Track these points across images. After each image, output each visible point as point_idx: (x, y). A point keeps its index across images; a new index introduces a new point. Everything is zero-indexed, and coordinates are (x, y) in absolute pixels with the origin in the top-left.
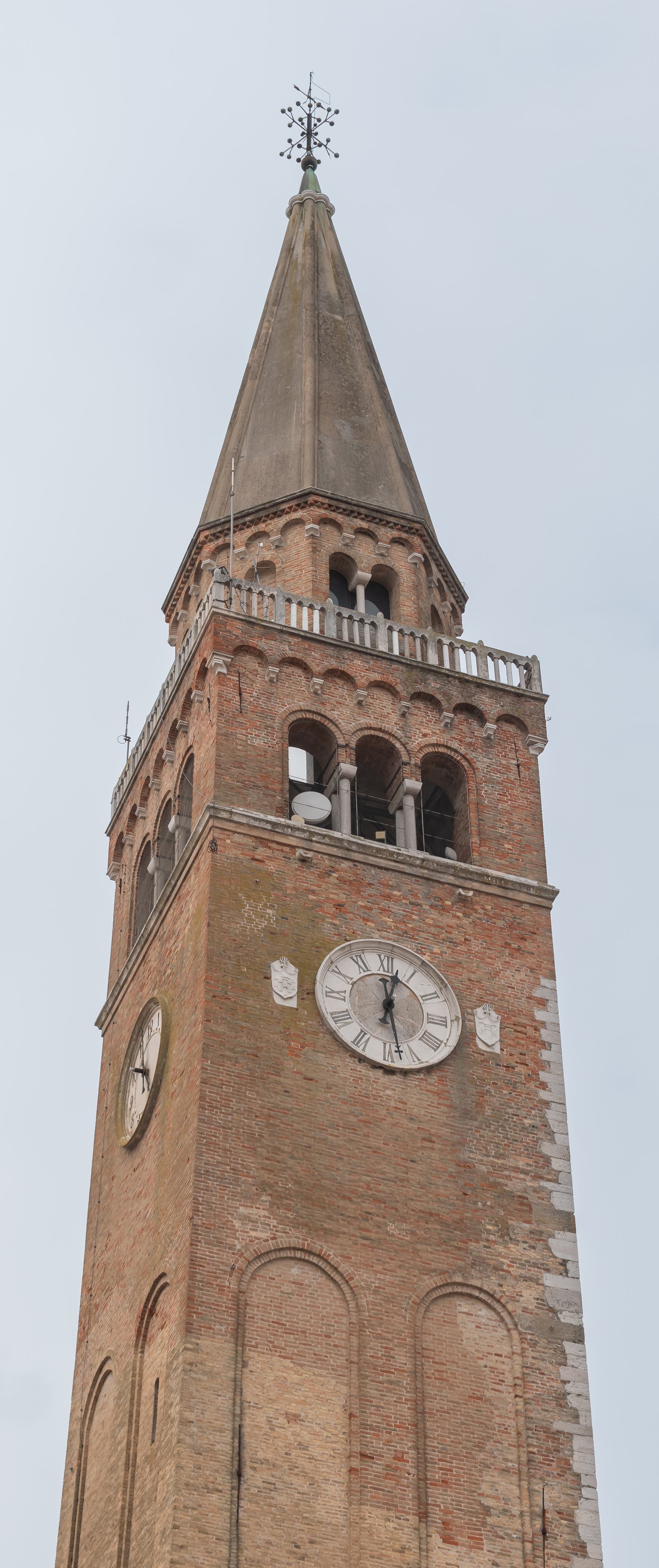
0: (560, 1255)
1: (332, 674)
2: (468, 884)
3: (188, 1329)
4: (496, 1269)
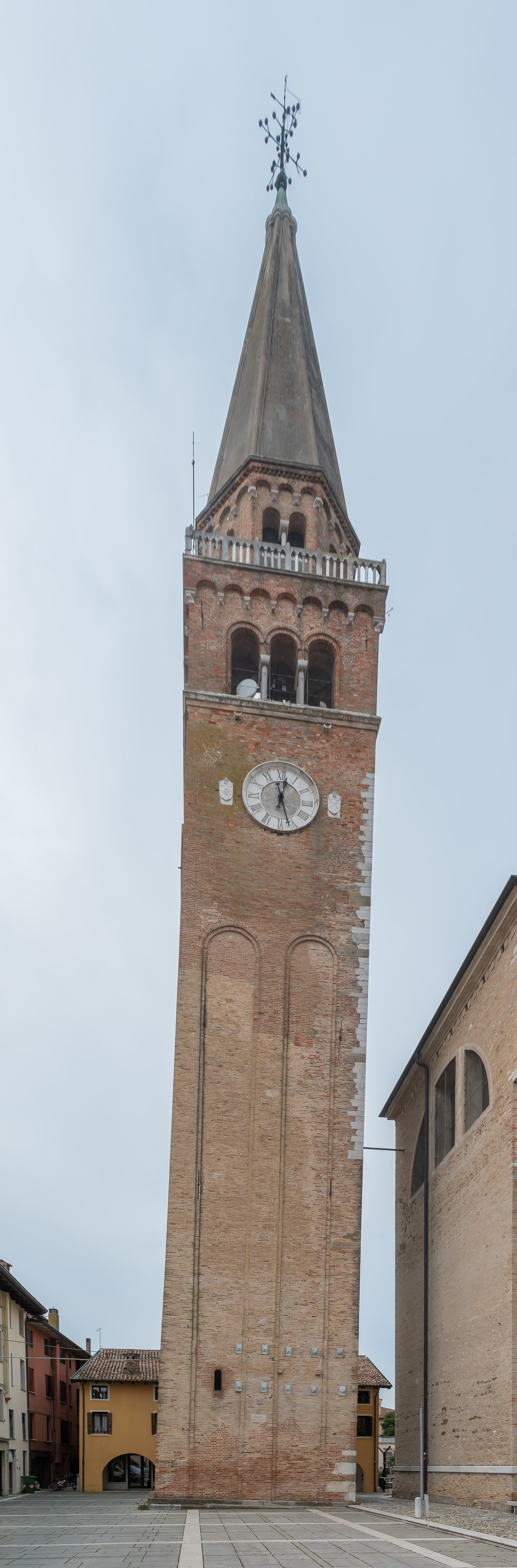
2: (330, 721)
4: (328, 927)
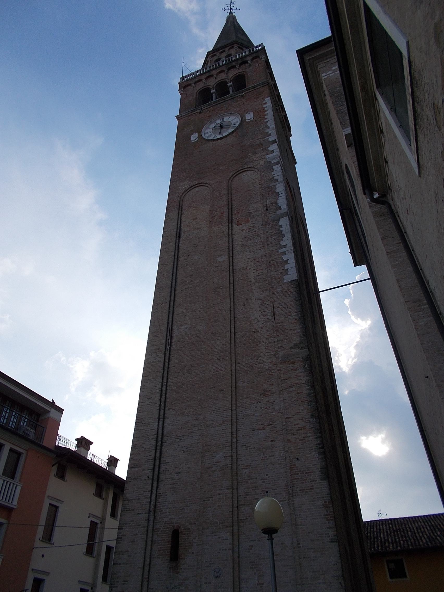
0: (271, 150)
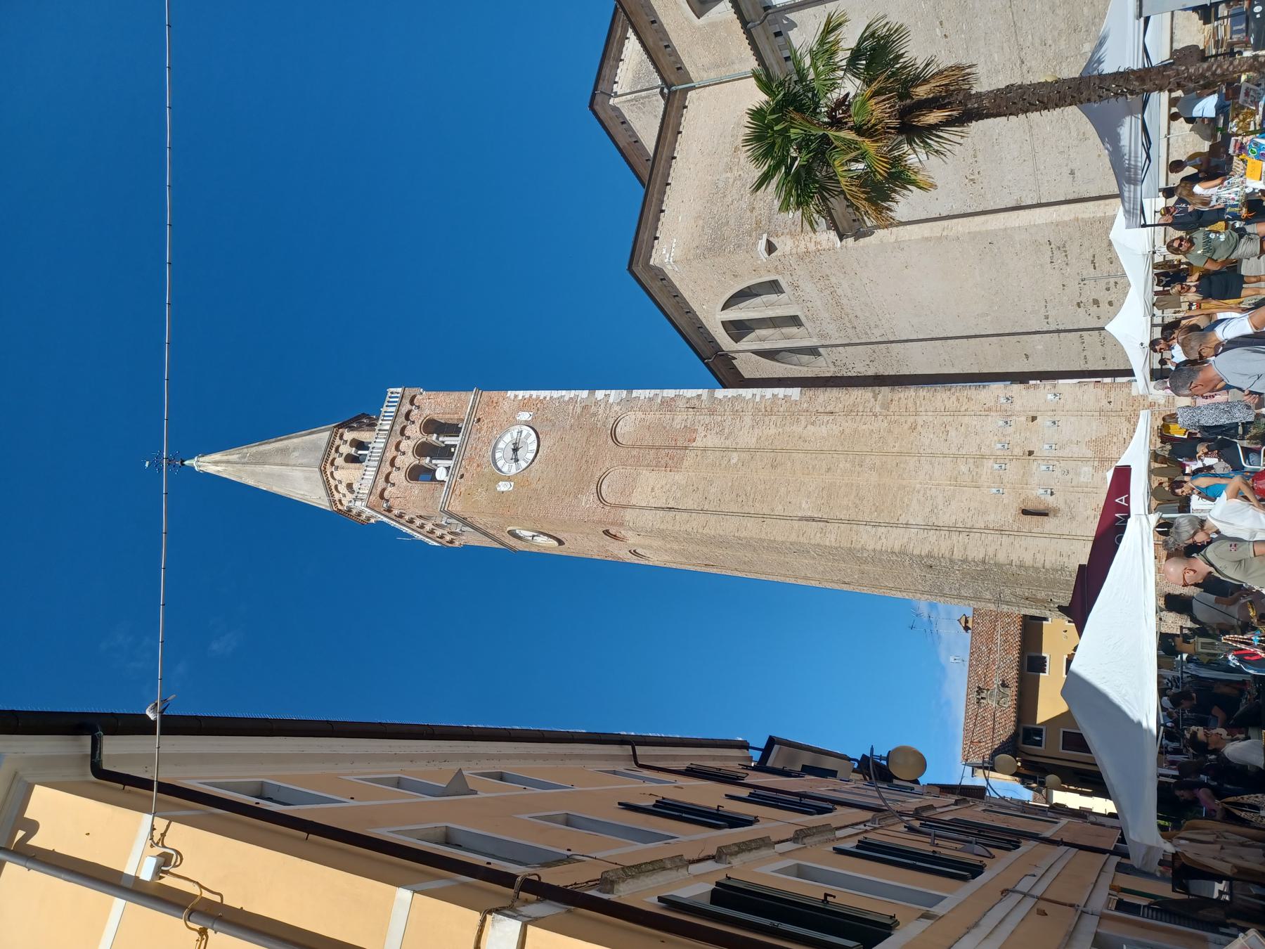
1: (392, 464)
3: (622, 525)
